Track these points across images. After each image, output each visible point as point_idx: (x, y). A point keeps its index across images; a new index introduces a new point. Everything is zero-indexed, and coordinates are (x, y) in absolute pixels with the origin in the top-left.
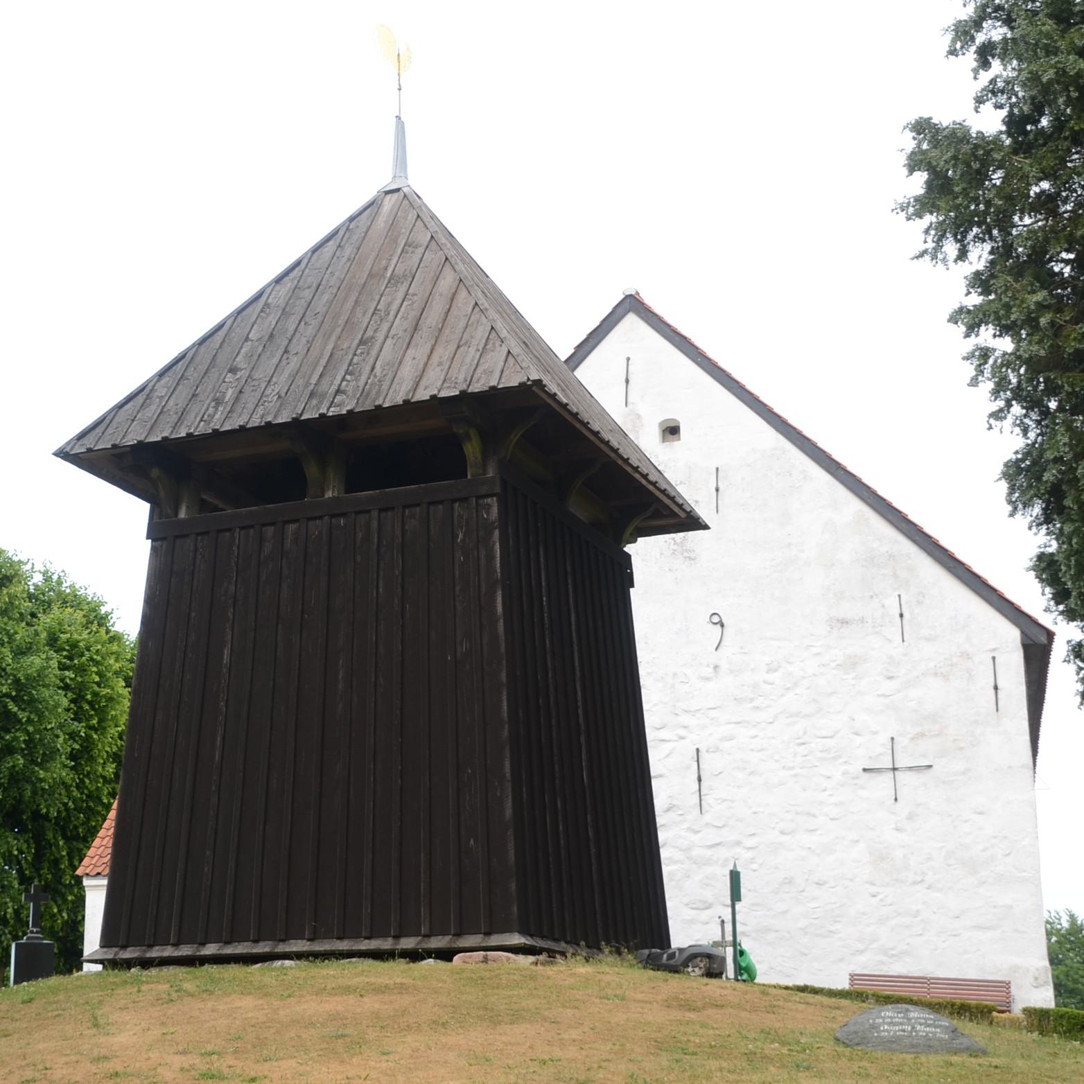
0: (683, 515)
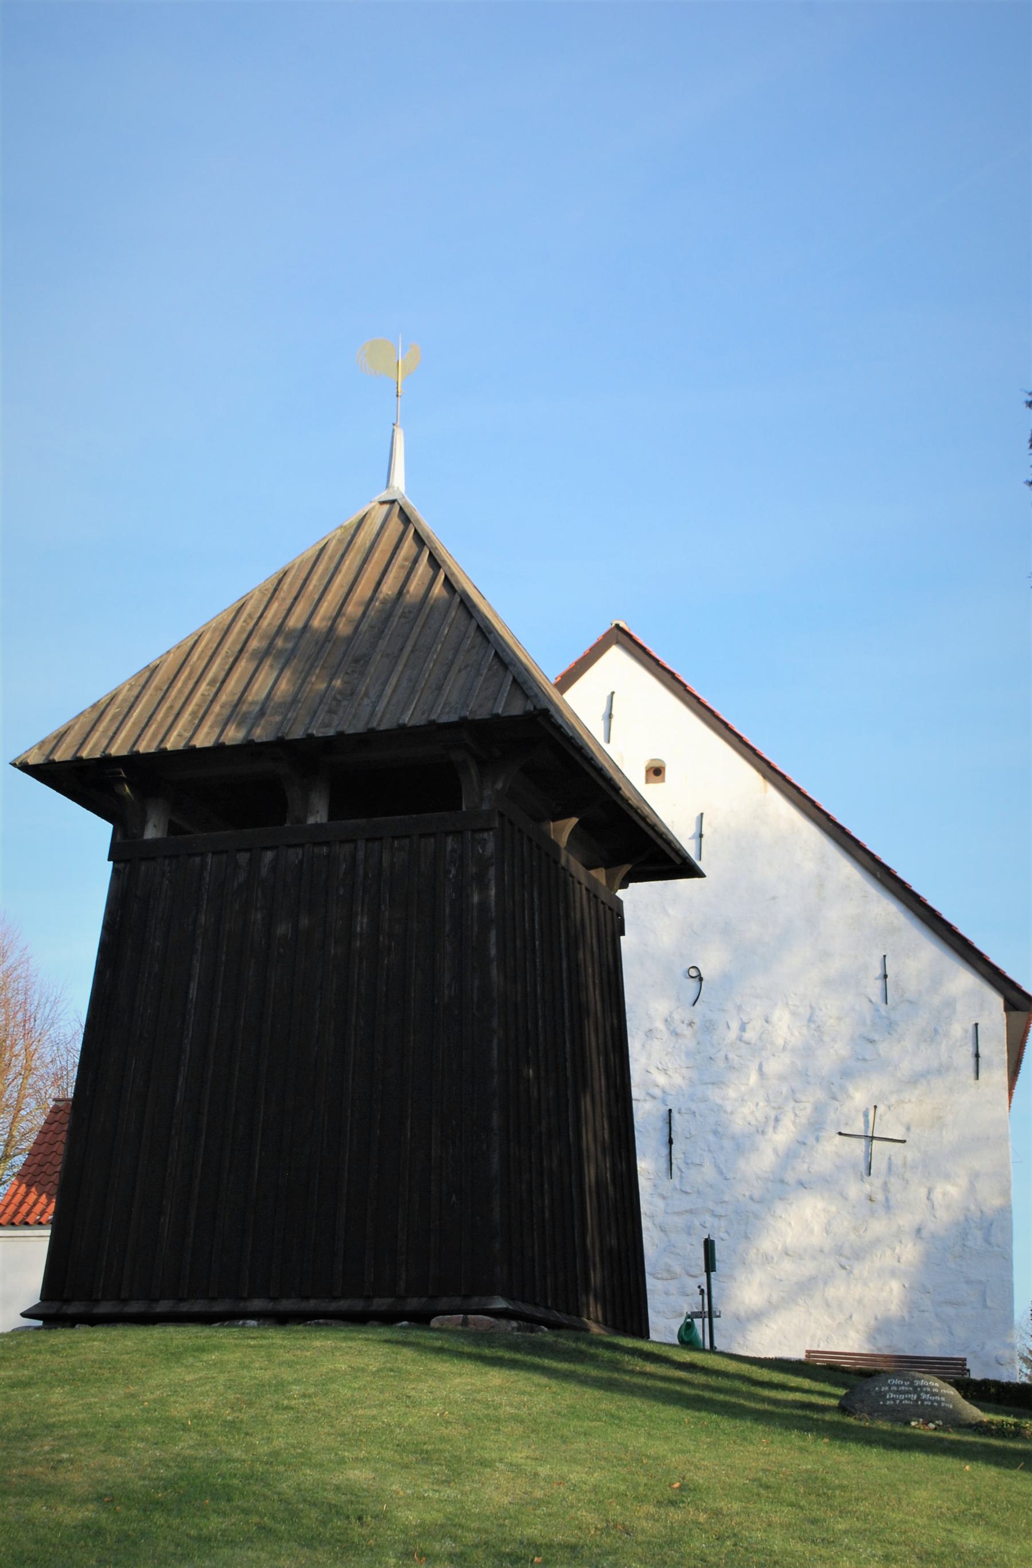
0: (678, 861)
